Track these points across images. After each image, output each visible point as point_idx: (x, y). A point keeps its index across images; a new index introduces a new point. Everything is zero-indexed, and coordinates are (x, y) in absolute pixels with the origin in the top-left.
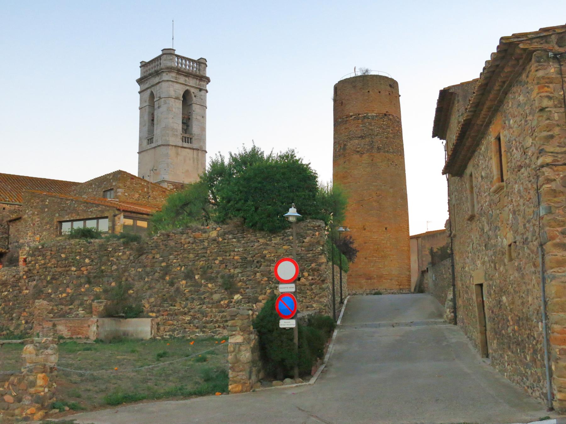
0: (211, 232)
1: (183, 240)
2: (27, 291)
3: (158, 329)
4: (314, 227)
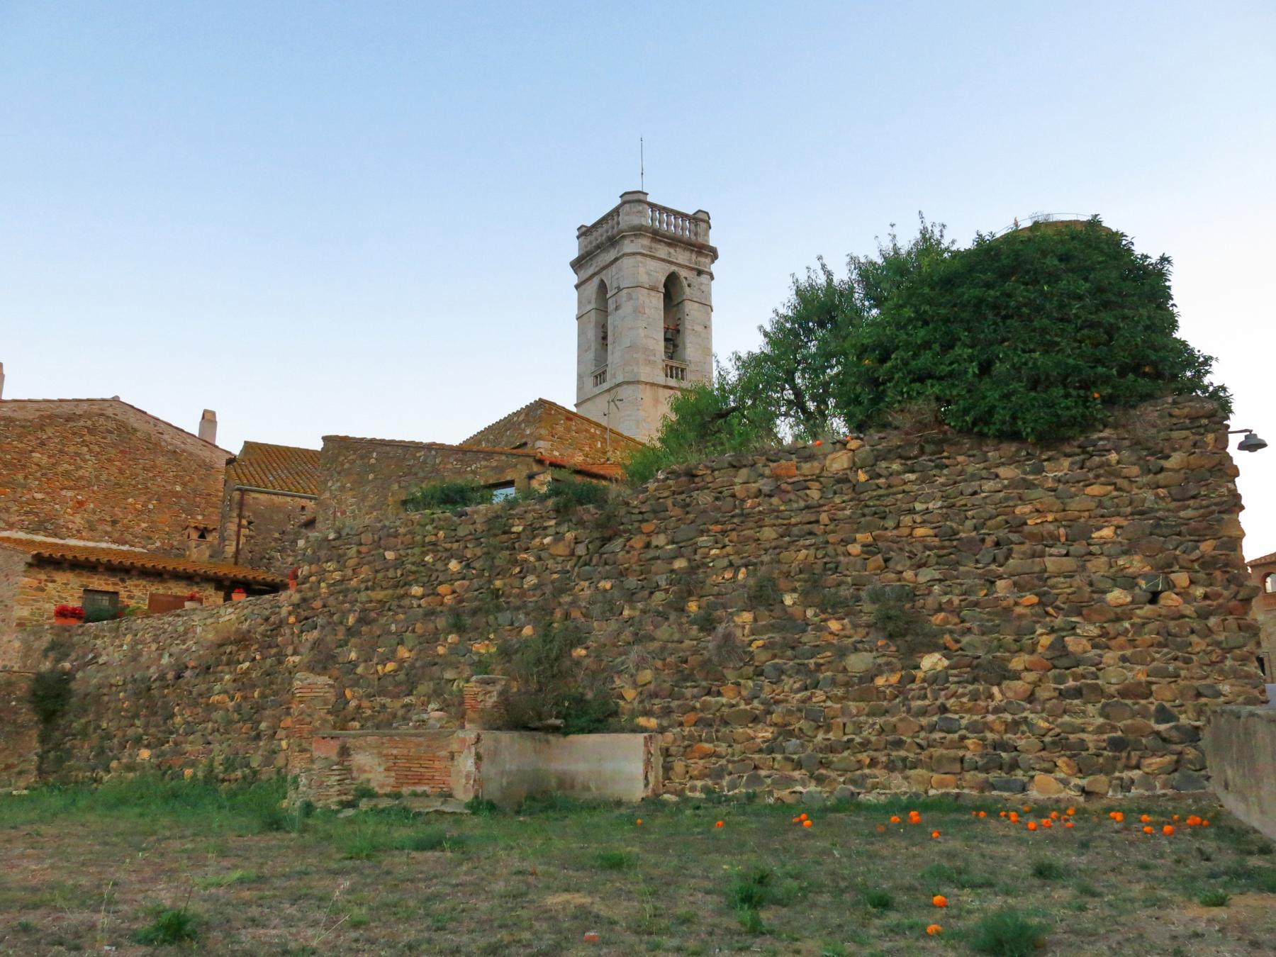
0: (830, 457)
1: (737, 488)
2: (297, 659)
3: (667, 769)
4: (1193, 419)
